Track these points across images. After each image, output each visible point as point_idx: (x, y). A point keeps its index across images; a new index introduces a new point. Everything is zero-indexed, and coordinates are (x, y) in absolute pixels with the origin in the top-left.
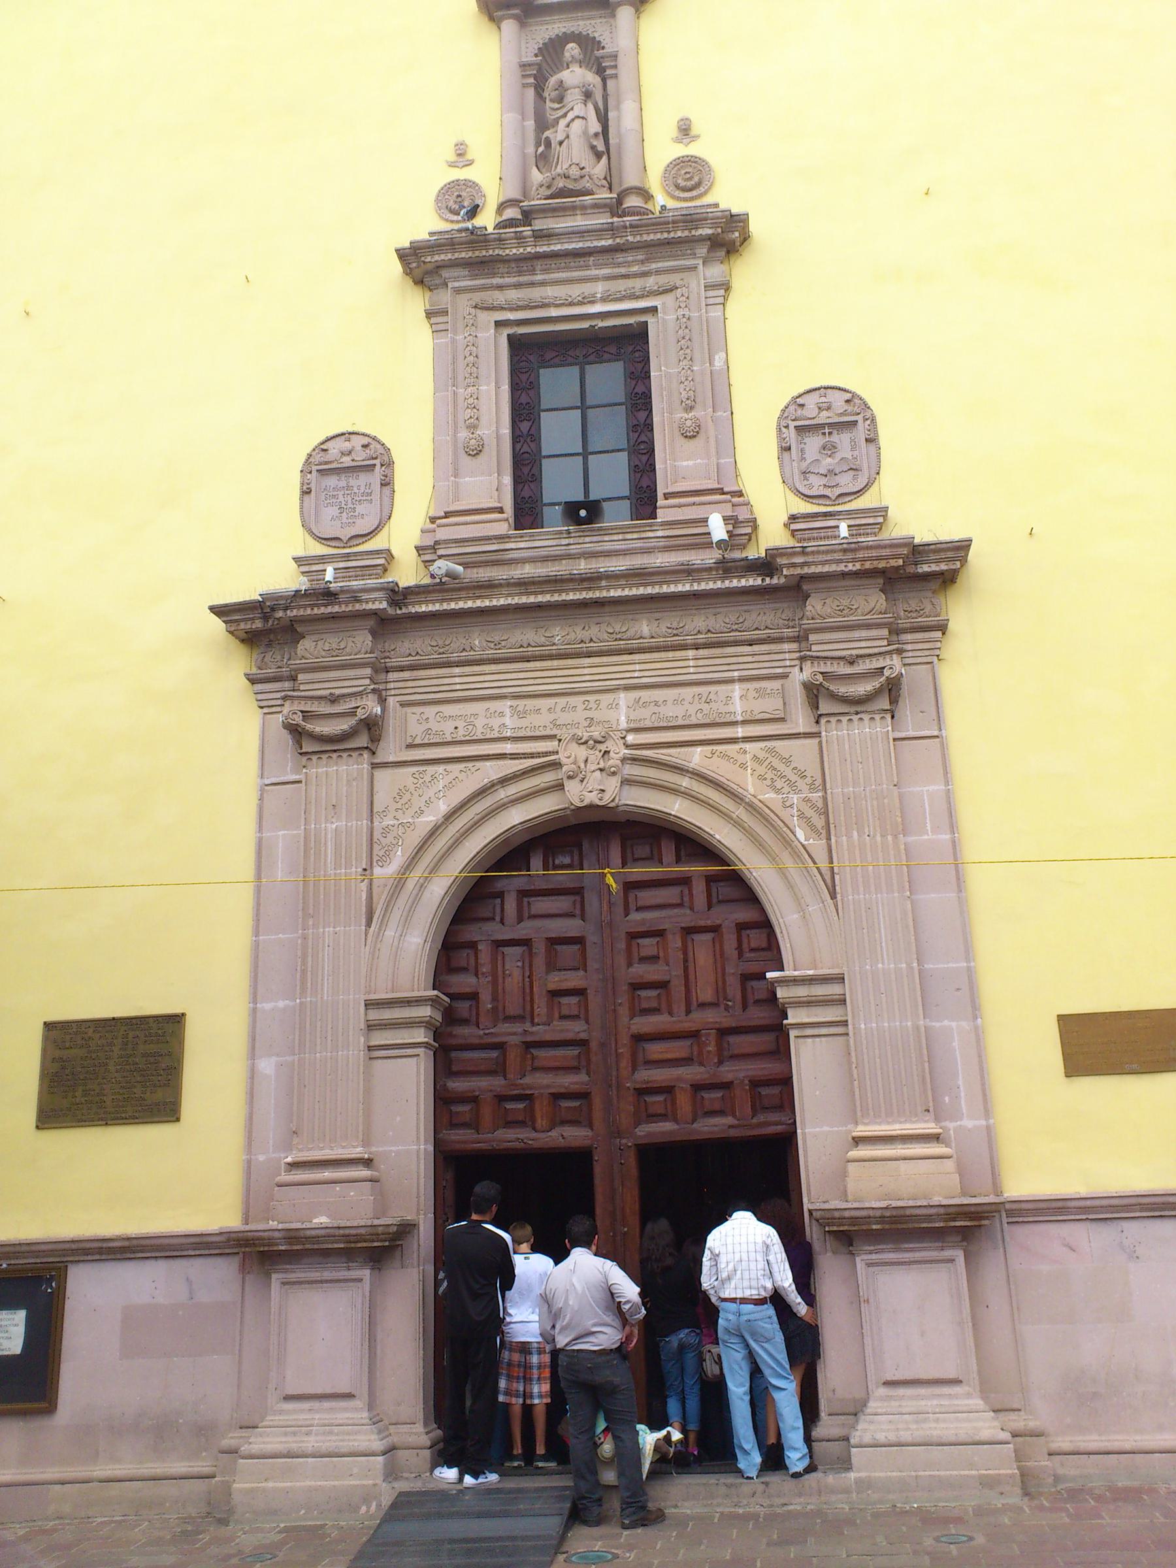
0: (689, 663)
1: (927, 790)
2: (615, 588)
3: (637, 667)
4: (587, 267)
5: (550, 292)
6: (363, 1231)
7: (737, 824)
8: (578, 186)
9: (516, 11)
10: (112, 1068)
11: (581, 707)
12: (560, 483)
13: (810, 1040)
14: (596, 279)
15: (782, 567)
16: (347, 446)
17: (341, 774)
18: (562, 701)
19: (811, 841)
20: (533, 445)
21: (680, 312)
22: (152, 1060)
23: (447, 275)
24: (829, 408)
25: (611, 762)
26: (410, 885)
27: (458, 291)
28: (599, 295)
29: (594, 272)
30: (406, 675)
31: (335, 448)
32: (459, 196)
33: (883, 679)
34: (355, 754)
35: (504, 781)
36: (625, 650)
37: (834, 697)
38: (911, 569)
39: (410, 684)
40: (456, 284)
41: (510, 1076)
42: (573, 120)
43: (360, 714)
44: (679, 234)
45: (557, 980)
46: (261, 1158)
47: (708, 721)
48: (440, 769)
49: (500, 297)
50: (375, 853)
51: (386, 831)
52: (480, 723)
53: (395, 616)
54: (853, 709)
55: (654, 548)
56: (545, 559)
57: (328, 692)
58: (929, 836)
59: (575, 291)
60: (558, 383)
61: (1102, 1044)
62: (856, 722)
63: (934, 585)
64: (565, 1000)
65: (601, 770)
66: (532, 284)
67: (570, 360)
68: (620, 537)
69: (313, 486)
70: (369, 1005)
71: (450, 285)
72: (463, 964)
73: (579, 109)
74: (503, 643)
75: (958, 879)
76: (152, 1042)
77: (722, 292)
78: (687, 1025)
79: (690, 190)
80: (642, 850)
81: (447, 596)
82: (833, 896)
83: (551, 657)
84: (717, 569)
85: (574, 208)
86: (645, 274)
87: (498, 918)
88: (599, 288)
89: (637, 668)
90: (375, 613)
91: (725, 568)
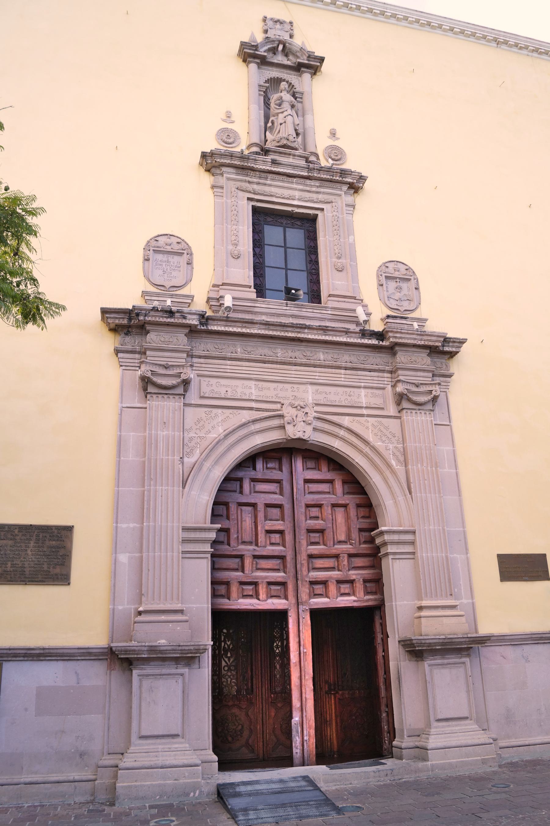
0: (342, 376)
1: (446, 449)
2: (312, 334)
3: (318, 374)
4: (292, 183)
5: (273, 190)
6: (192, 648)
7: (366, 456)
8: (292, 145)
9: (258, 61)
10: (29, 553)
11: (290, 390)
12: (273, 279)
13: (398, 561)
14: (296, 189)
15: (390, 337)
16: (169, 241)
17: (164, 407)
18: (281, 386)
19: (398, 467)
20: (261, 260)
21: (335, 213)
22: (54, 550)
23: (225, 170)
24: (398, 271)
25: (308, 418)
26: (205, 469)
27: (228, 179)
28: (297, 197)
29: (295, 186)
30: (202, 360)
31: (162, 240)
32: (228, 136)
33: (432, 396)
34: (177, 397)
35: (254, 421)
36: (313, 365)
37: (409, 400)
38: (441, 349)
39: (204, 365)
40: (228, 176)
41: (247, 572)
42: (287, 116)
43: (183, 377)
44: (338, 178)
45: (270, 525)
46: (120, 608)
47: (350, 405)
48: (220, 411)
49: (250, 187)
50: (185, 450)
51: (191, 439)
52: (239, 390)
53: (200, 329)
54: (417, 407)
55: (325, 319)
56: (273, 315)
57: (166, 363)
58: (446, 470)
59: (286, 193)
60: (273, 233)
61: (518, 567)
62: (409, 414)
63: (447, 357)
64: (273, 535)
65: (304, 421)
66: (265, 184)
67: (279, 224)
68: (311, 310)
69: (151, 257)
70: (185, 529)
71: (225, 175)
72: (221, 513)
73: (289, 112)
74: (252, 352)
75: (459, 490)
76: (54, 540)
77: (352, 209)
78: (334, 552)
79: (336, 161)
80: (311, 464)
81: (229, 324)
82: (410, 493)
83: (277, 363)
84: (359, 333)
85: (290, 154)
86: (317, 193)
87: (238, 490)
88: (297, 194)
89: (318, 374)
90: (189, 326)
91: (364, 333)
